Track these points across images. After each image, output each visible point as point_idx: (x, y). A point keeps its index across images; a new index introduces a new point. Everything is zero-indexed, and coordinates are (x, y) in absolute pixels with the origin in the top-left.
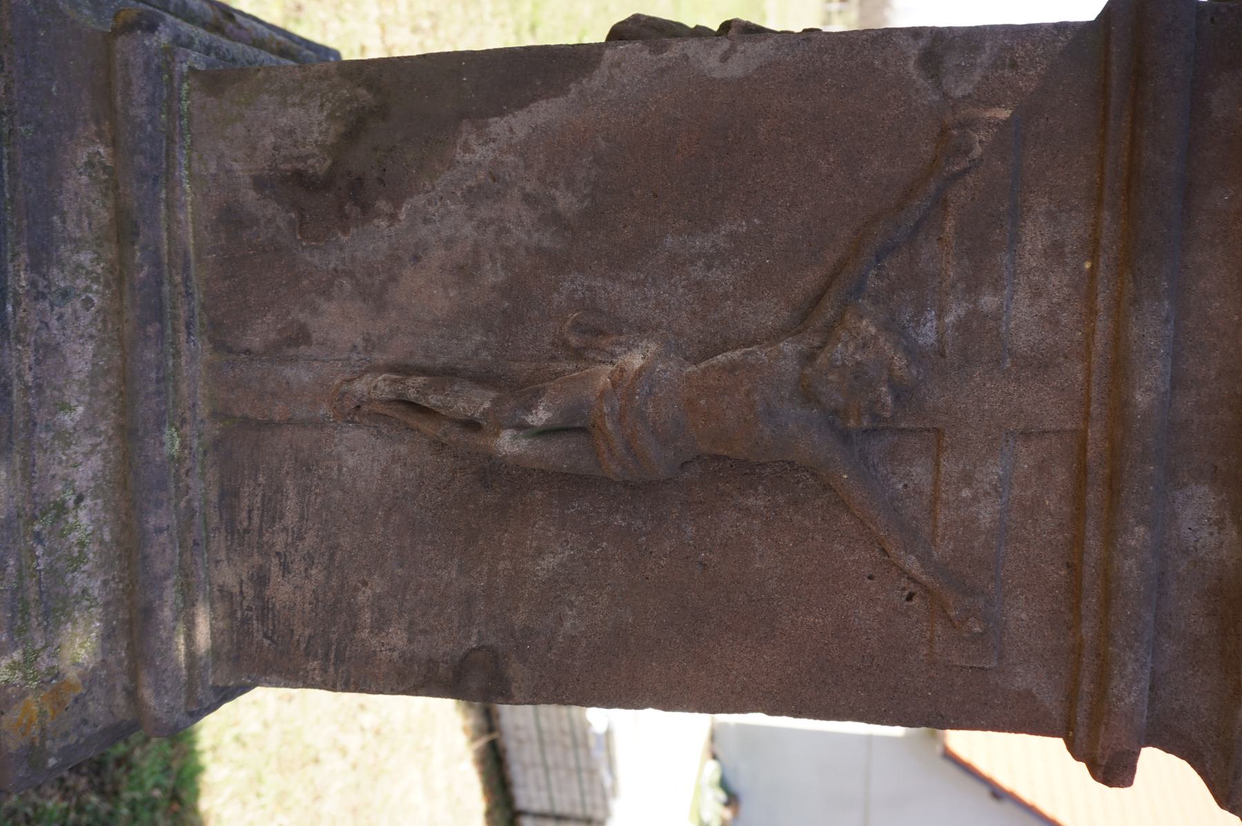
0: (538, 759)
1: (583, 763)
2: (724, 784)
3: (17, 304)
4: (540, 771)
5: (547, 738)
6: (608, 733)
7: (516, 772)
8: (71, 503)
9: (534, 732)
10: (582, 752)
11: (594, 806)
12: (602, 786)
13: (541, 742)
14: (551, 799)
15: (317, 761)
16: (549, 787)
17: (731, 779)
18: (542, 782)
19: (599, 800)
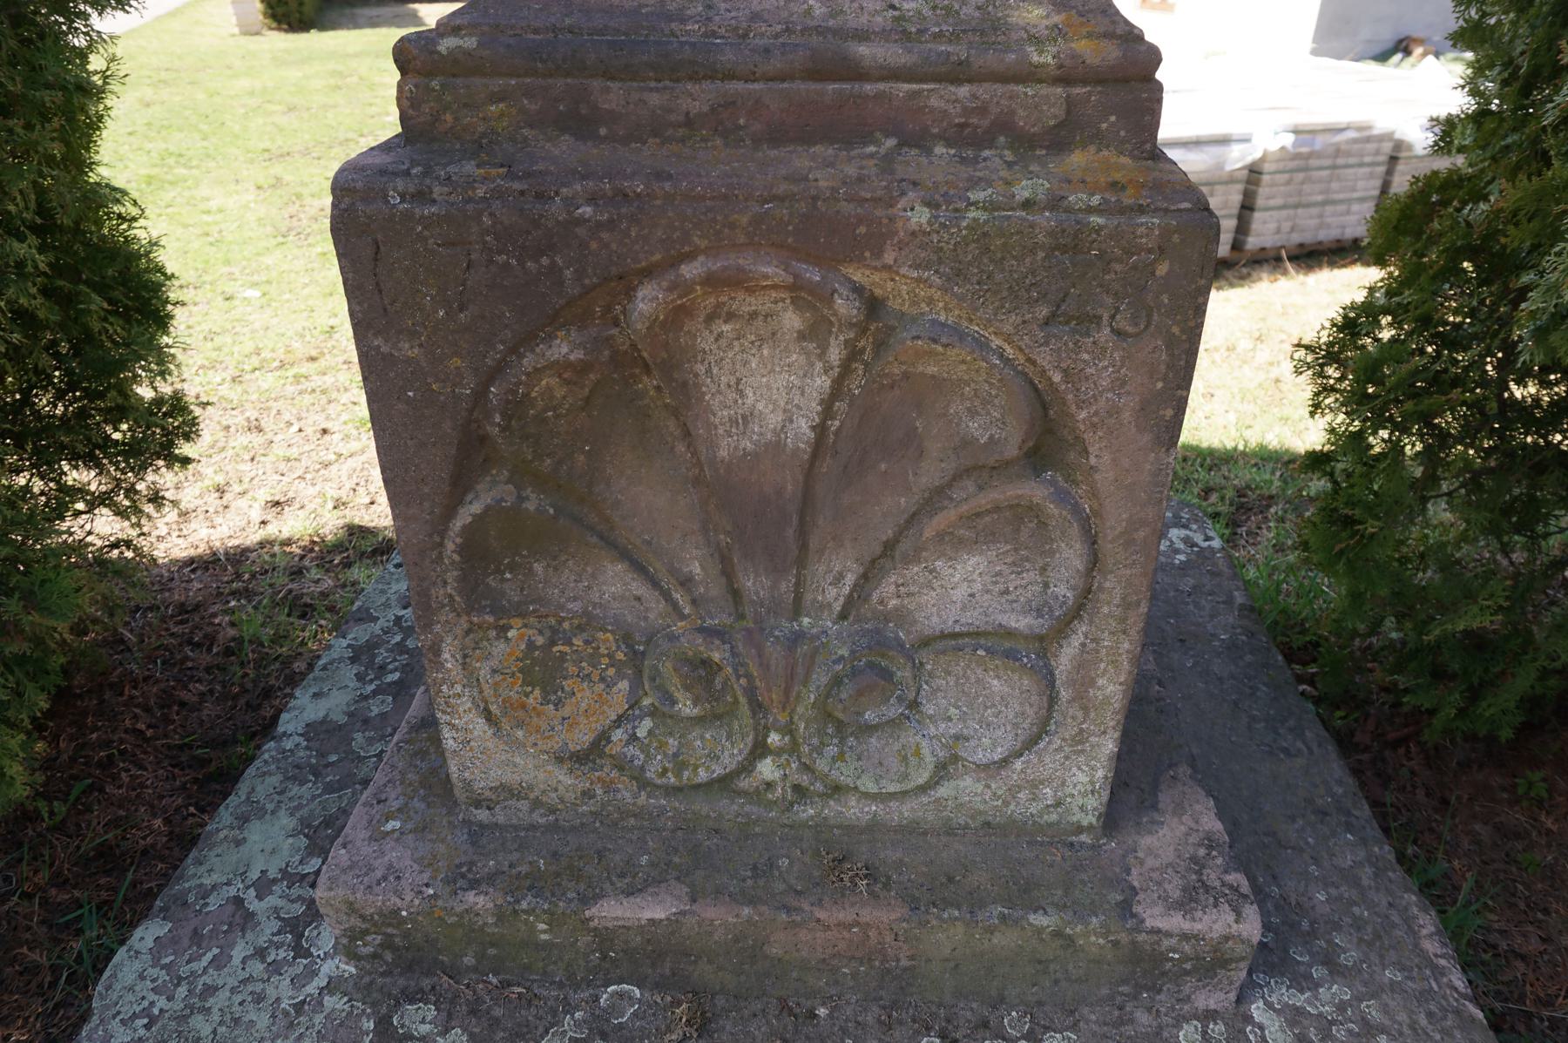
0: (1314, 211)
1: (1327, 162)
2: (1382, 57)
3: (714, 34)
4: (1329, 209)
5: (1291, 200)
6: (1296, 131)
7: (1327, 235)
8: (896, 13)
9: (1284, 213)
10: (1314, 162)
11: (1377, 153)
12: (1355, 141)
13: (1296, 206)
14: (1362, 200)
15: (1277, 381)
16: (1349, 201)
17: (1377, 49)
18: (1341, 208)
19: (1371, 147)
